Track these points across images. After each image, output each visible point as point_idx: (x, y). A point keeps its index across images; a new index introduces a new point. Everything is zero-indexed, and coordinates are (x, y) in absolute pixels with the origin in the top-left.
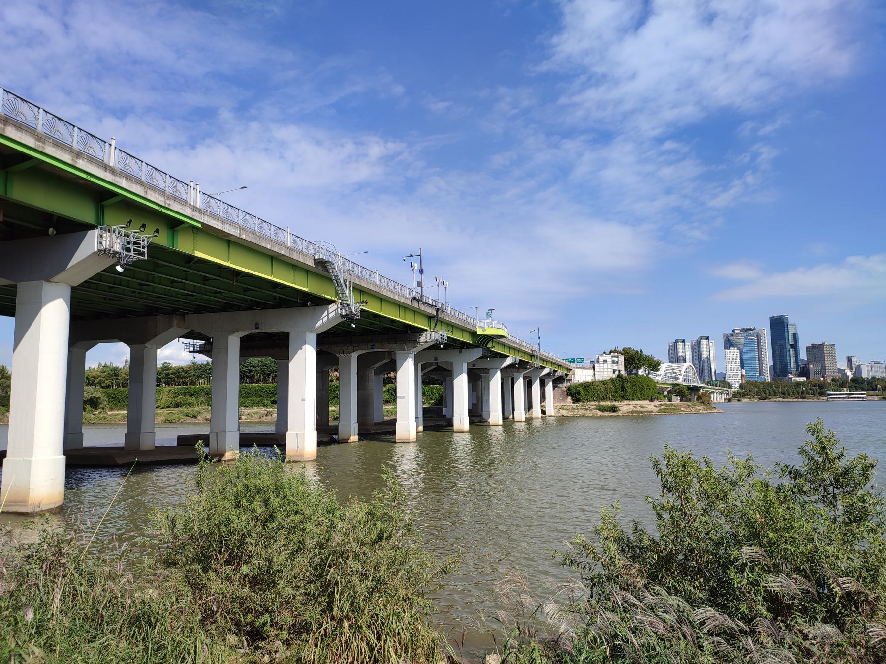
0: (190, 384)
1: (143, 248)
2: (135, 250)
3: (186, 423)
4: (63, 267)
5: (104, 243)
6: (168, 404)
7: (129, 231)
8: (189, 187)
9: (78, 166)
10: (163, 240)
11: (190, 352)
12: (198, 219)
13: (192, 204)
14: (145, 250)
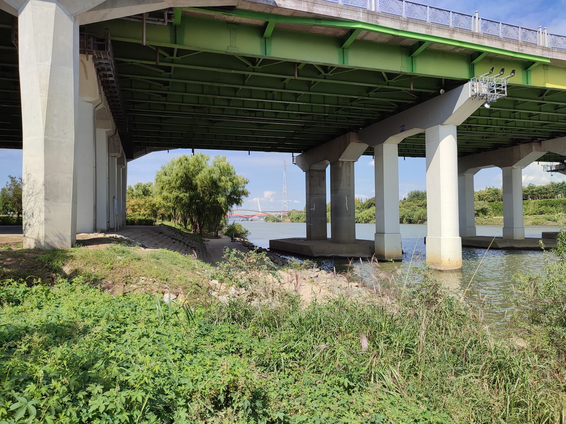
0: (550, 198)
1: (504, 87)
2: (497, 90)
3: (549, 225)
4: (450, 114)
5: (475, 90)
6: (534, 212)
7: (492, 77)
8: (538, 32)
9: (454, 39)
10: (518, 79)
11: (548, 171)
12: (547, 57)
13: (541, 45)
14: (505, 89)
